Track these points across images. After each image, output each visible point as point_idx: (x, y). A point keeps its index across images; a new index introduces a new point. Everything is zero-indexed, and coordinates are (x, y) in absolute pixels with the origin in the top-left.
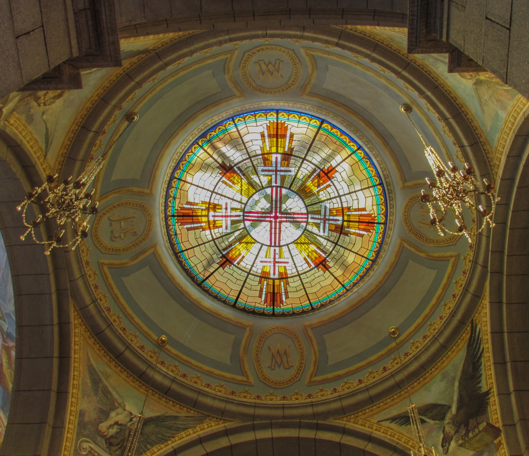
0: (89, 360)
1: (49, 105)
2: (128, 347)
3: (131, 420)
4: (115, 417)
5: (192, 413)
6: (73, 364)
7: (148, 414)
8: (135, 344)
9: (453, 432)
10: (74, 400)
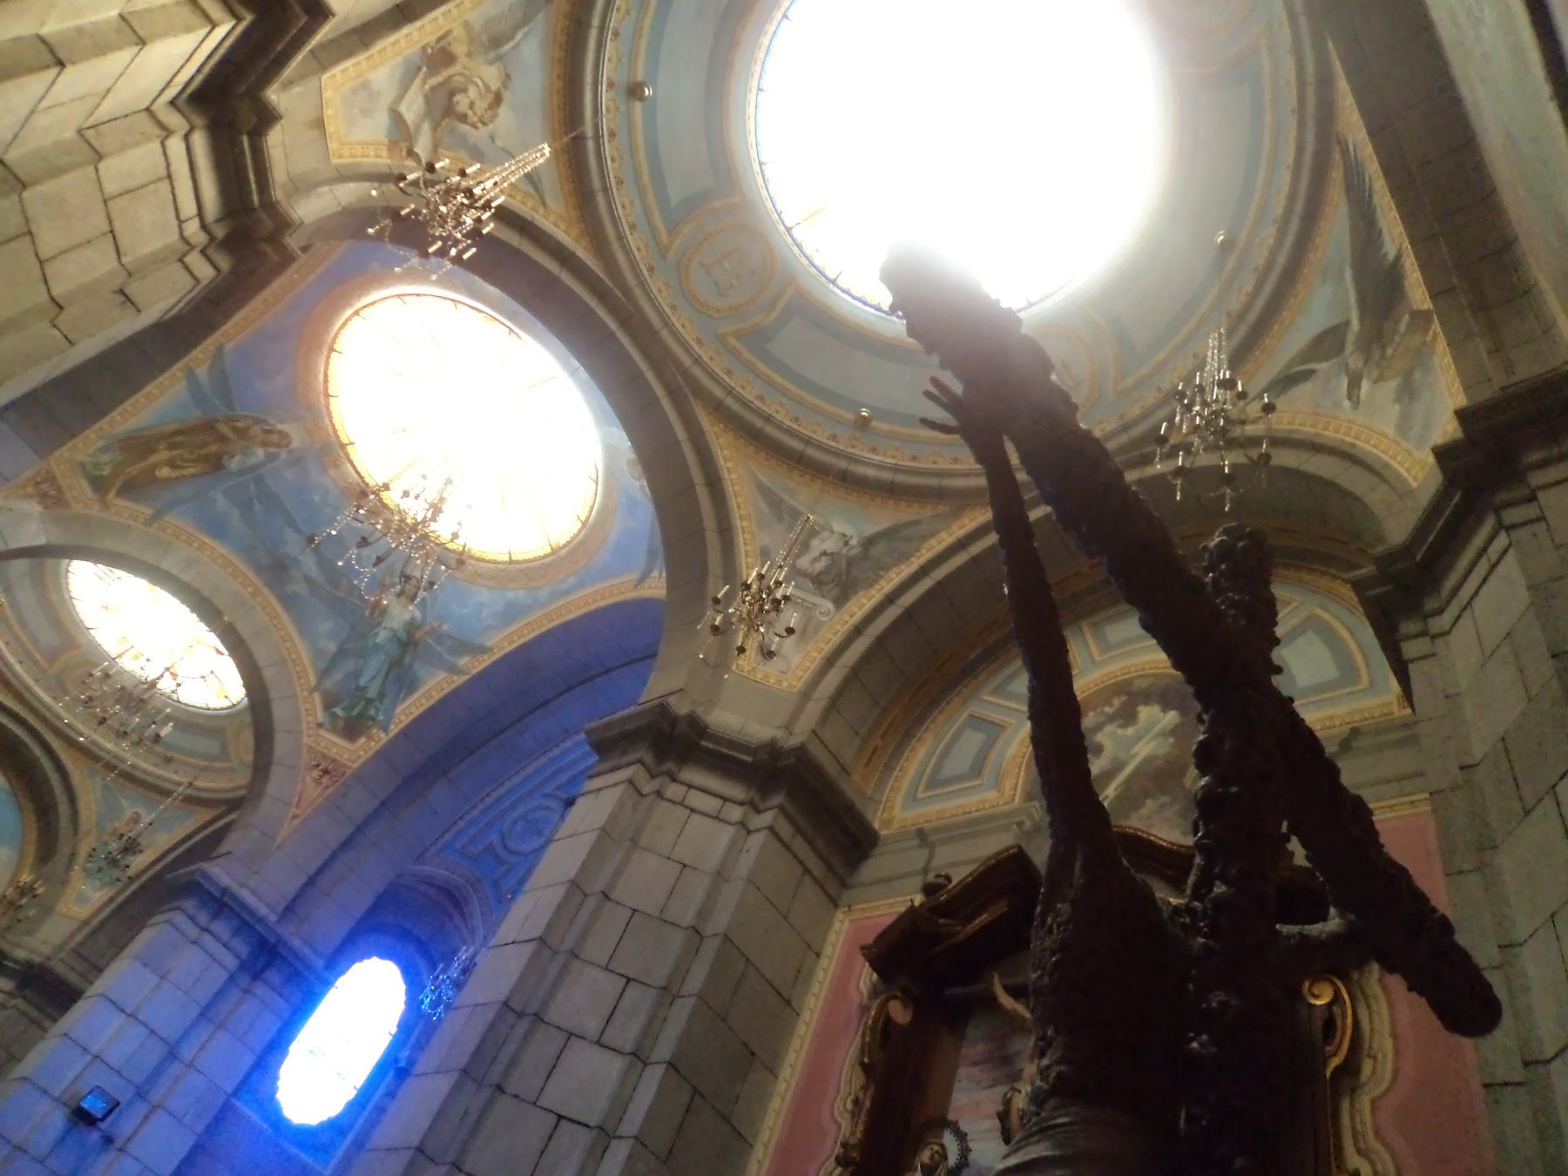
0: (756, 477)
1: (492, 121)
2: (808, 442)
3: (846, 543)
4: (817, 546)
5: (942, 508)
6: (729, 488)
7: (871, 529)
8: (821, 436)
9: (1360, 364)
10: (746, 536)
